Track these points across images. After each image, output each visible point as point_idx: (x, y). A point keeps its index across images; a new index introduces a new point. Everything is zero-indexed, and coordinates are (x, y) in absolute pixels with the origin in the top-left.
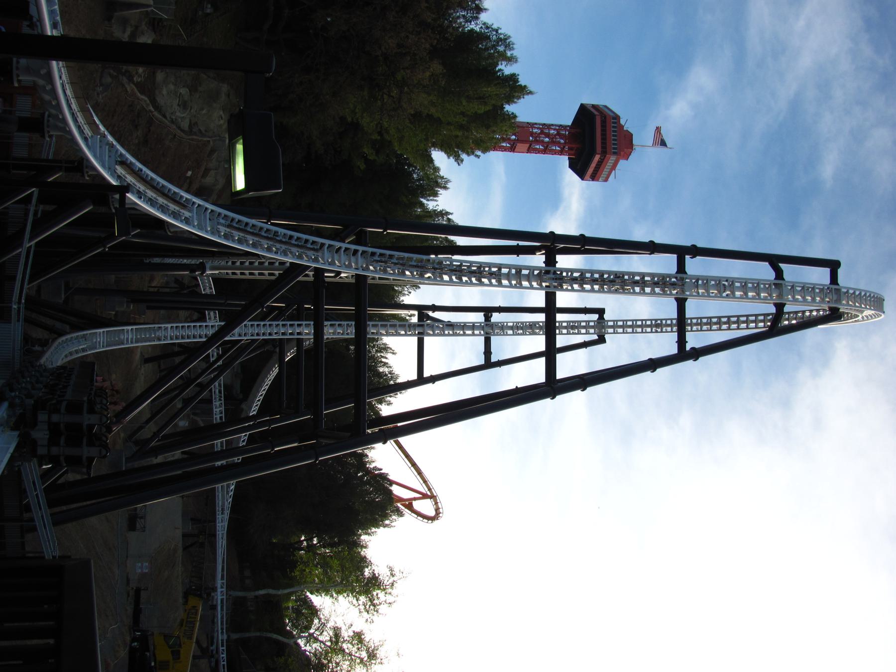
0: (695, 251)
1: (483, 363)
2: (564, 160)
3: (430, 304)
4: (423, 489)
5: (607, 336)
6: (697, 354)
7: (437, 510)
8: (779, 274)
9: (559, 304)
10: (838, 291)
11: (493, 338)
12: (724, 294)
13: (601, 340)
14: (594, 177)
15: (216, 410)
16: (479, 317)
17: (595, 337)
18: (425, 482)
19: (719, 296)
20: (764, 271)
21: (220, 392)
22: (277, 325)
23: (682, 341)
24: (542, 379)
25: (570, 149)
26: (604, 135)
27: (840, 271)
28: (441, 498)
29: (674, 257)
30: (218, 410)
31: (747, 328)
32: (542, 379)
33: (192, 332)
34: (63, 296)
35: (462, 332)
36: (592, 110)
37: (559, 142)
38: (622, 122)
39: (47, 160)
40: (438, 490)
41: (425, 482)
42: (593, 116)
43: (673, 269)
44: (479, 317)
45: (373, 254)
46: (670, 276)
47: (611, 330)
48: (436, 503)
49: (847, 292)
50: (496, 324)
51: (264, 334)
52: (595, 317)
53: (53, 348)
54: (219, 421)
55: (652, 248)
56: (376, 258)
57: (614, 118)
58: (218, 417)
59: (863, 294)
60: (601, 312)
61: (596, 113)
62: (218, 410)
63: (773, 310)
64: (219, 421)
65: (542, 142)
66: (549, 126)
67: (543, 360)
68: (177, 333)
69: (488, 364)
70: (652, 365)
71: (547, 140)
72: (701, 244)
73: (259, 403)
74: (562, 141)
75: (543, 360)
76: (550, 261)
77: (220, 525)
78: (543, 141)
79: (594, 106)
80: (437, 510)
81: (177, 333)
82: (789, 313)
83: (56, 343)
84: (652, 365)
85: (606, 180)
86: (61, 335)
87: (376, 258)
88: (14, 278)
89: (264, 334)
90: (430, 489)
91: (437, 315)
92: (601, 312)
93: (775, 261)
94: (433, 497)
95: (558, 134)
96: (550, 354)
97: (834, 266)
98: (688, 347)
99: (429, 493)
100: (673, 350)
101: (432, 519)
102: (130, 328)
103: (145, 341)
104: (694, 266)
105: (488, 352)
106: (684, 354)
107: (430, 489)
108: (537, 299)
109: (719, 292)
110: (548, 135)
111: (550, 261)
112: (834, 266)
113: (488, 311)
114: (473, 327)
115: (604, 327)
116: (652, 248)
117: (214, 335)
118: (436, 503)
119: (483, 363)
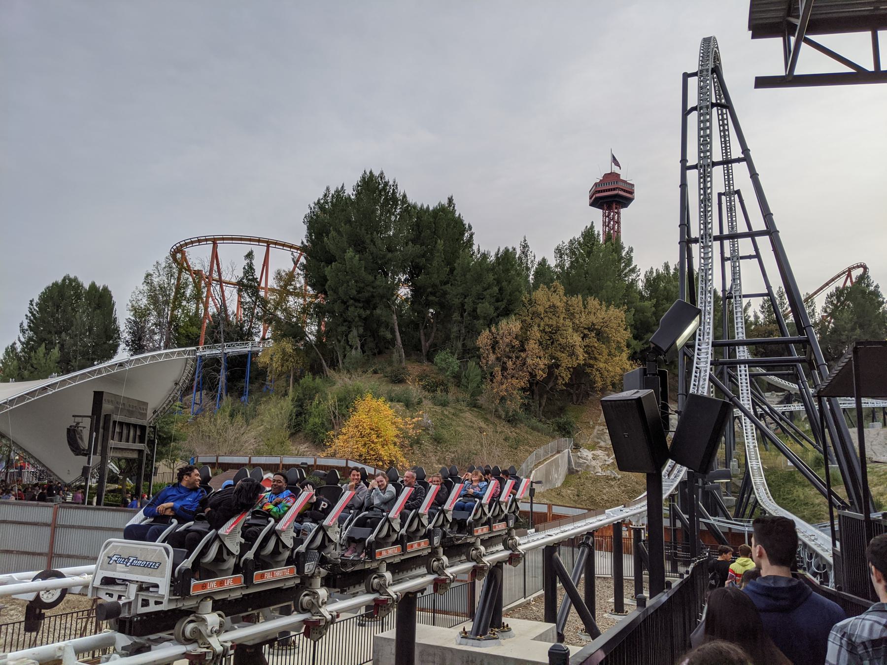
0: (684, 160)
1: (757, 259)
2: (623, 211)
3: (679, 189)
4: (844, 277)
5: (735, 190)
6: (745, 150)
7: (858, 267)
8: (694, 109)
9: (718, 234)
10: (701, 71)
11: (741, 255)
12: (709, 140)
13: (738, 192)
14: (632, 193)
15: (797, 409)
16: (728, 264)
17: (736, 196)
18: (839, 276)
19: (710, 143)
20: (693, 118)
21: (785, 407)
22: (741, 379)
23: (738, 160)
24: (767, 237)
25: (616, 208)
26: (604, 191)
27: (689, 72)
28: (850, 265)
29: (688, 172)
30: (797, 408)
31: (727, 119)
32: (767, 237)
33: (749, 431)
34: (732, 498)
35: (738, 268)
36: (593, 199)
37: (613, 215)
38: (598, 181)
39: (670, 510)
40: (845, 267)
41: (839, 276)
42: (596, 198)
43: (695, 171)
44: (728, 264)
45: (699, 340)
46: (700, 174)
47: (732, 187)
48: (854, 268)
49: (701, 61)
50: (731, 254)
51: (747, 387)
52: (723, 198)
53: (767, 508)
54: (803, 407)
55: (684, 185)
56: (701, 338)
57: (596, 186)
58: (801, 407)
59: (702, 51)
60: (720, 195)
61: (594, 197)
62: (797, 408)
63: (715, 109)
64: (803, 407)
65: (614, 225)
66: (604, 223)
67: (757, 238)
68: (750, 437)
69: (758, 256)
70: (754, 176)
71: (612, 223)
72: (679, 182)
73: (790, 383)
74: (612, 214)
75: (757, 238)
76: (696, 241)
77: (876, 404)
78: (613, 225)
79: (591, 198)
80: (858, 267)
81: (750, 437)
82: (716, 100)
83: (761, 504)
84: (754, 176)
85: (633, 185)
86: (757, 501)
87: (701, 338)
88: (730, 528)
89: (747, 387)
90: (844, 273)
91: (728, 286)
92: (720, 195)
93: (686, 113)
94: (850, 270)
95: (608, 216)
96: (752, 235)
97: (686, 76)
98: (742, 156)
99: (847, 273)
100: (744, 164)
101: (865, 268)
102: (749, 463)
103: (757, 454)
104: (692, 159)
105: (750, 257)
106: (746, 158)
107: (844, 273)
108: (717, 244)
109: (708, 143)
110: (609, 223)
111: (696, 241)
112: (686, 76)
113: (724, 259)
114: (734, 267)
115: (730, 193)
116: (684, 185)
117: (750, 419)
118: (854, 268)
119: (757, 259)
